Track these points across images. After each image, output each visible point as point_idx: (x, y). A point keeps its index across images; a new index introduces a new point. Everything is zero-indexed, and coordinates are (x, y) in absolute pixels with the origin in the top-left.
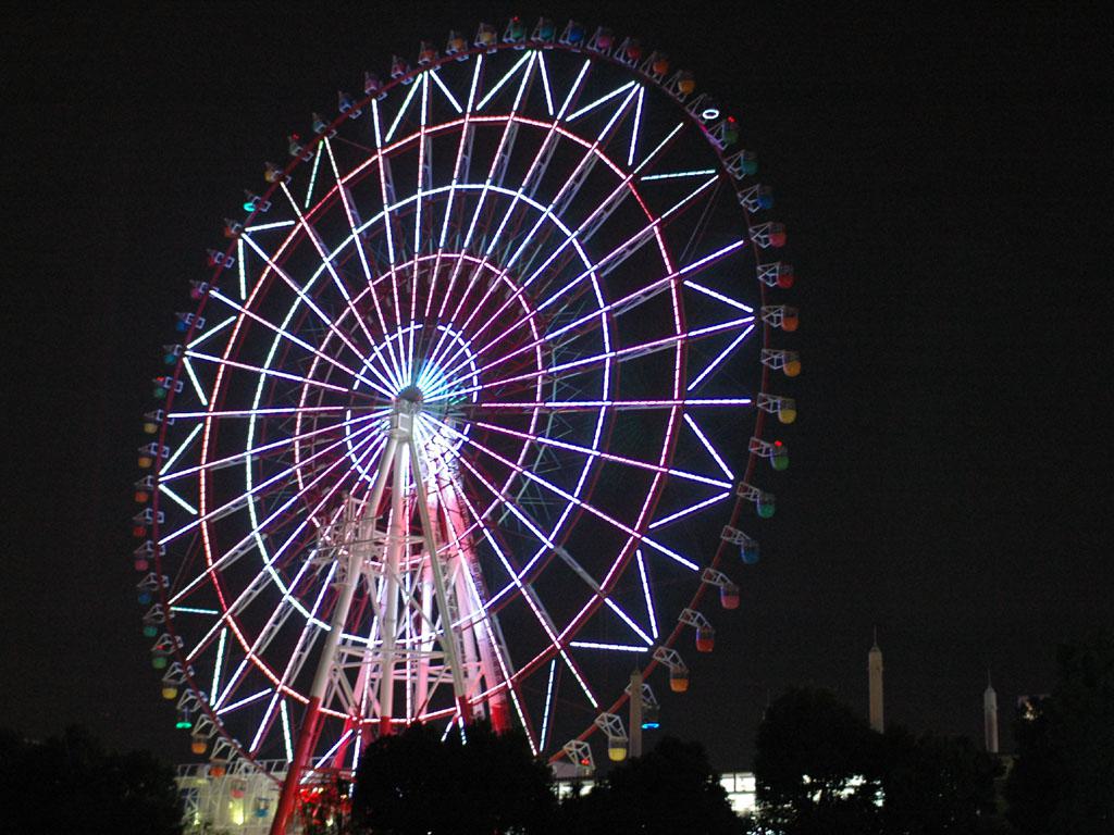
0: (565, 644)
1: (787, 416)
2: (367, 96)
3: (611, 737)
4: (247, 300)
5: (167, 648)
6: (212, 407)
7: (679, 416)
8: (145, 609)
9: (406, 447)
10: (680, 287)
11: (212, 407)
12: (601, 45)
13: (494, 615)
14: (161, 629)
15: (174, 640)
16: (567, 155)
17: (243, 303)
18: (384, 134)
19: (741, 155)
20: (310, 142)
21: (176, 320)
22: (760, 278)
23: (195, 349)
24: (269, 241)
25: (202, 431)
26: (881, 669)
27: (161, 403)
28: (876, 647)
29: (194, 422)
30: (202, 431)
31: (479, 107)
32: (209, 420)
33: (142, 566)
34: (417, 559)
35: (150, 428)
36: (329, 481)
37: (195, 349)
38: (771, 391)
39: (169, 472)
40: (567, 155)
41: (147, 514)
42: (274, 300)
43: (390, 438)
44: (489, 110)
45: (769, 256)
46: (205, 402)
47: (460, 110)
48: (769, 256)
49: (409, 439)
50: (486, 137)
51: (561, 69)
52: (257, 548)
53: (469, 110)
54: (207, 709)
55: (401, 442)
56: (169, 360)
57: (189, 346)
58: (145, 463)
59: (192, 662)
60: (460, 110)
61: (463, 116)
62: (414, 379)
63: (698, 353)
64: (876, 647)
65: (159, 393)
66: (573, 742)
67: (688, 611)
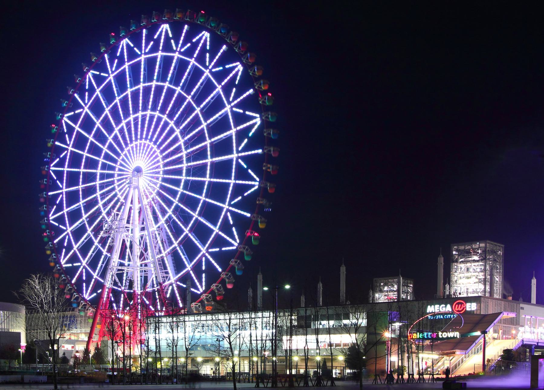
0: (207, 251)
2: (102, 53)
4: (70, 143)
6: (64, 187)
7: (237, 161)
9: (137, 190)
10: (232, 112)
11: (64, 187)
13: (181, 246)
16: (182, 65)
17: (68, 145)
18: (111, 67)
23: (54, 166)
24: (75, 119)
25: (62, 198)
26: (345, 273)
28: (343, 265)
29: (58, 195)
30: (62, 198)
32: (64, 193)
34: (143, 233)
36: (113, 207)
37: (253, 186)
39: (53, 215)
40: (182, 65)
41: (47, 233)
42: (80, 142)
43: (130, 187)
44: (151, 51)
46: (61, 186)
49: (137, 187)
50: (151, 63)
51: (176, 30)
52: (91, 238)
54: (84, 299)
55: (134, 188)
56: (44, 173)
57: (52, 165)
58: (43, 213)
59: (75, 283)
60: (139, 53)
63: (241, 135)
64: (343, 265)
67: (249, 231)
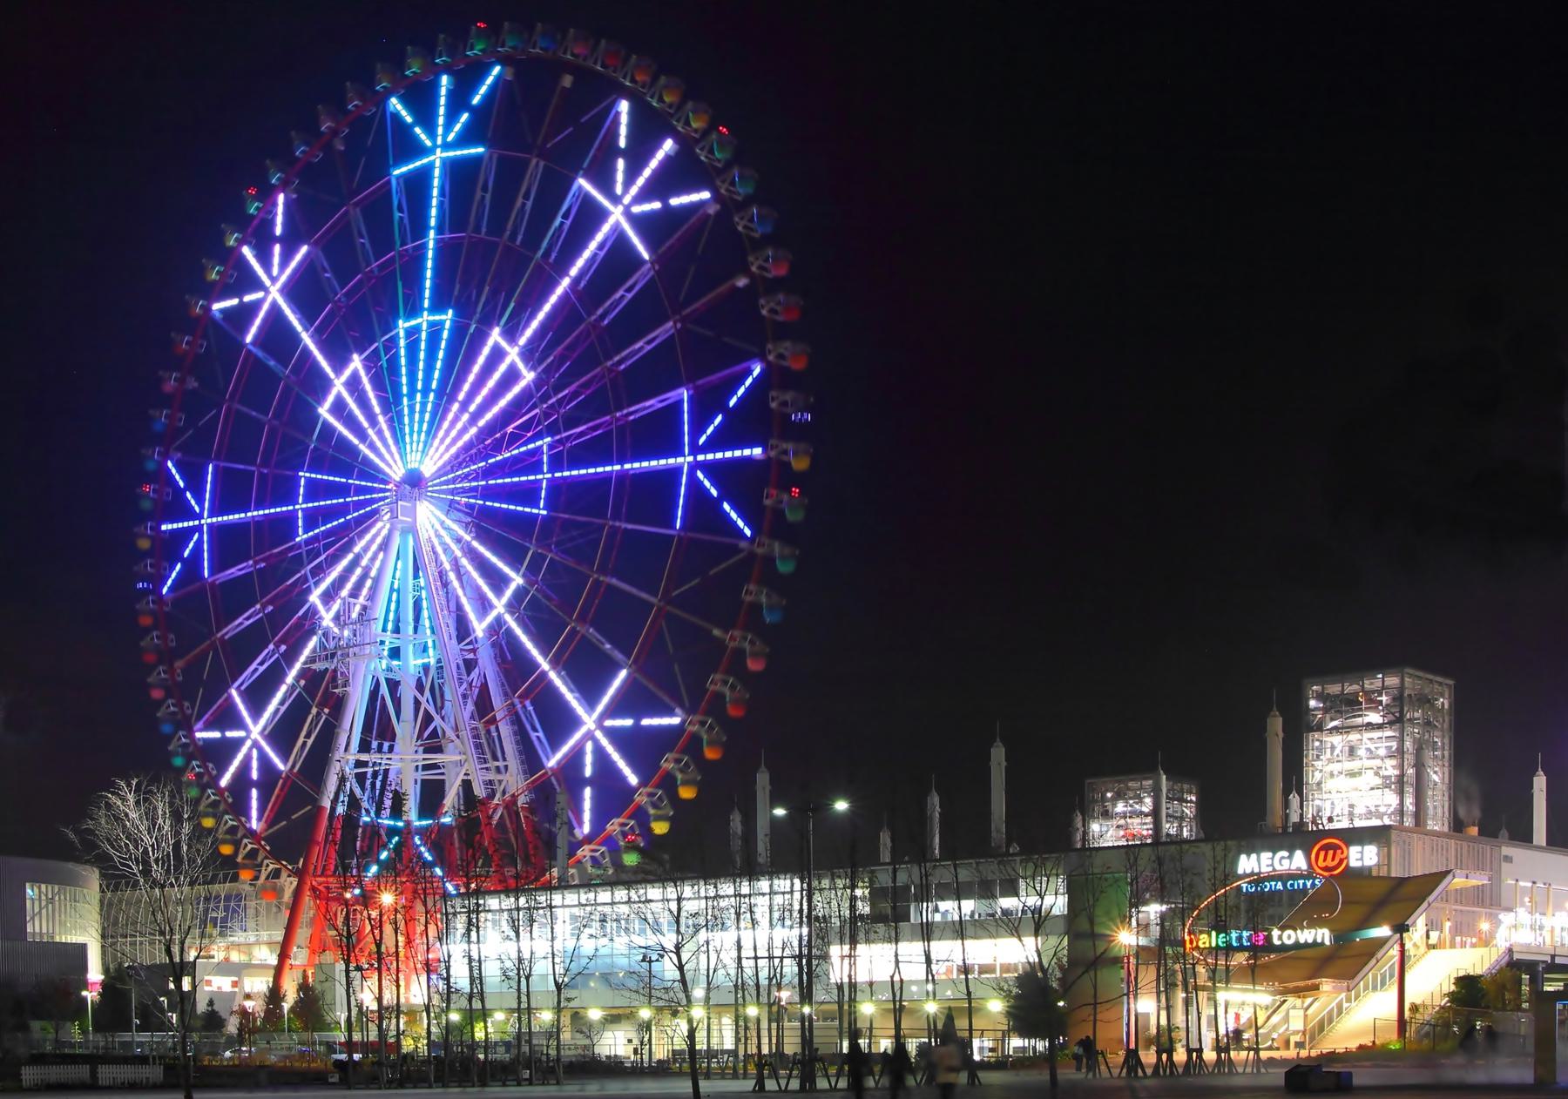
1: (800, 464)
3: (652, 811)
5: (199, 775)
8: (169, 738)
12: (576, 51)
14: (189, 758)
15: (206, 768)
19: (736, 171)
20: (267, 195)
21: (202, 271)
22: (764, 312)
25: (200, 540)
26: (1004, 764)
27: (144, 517)
28: (998, 743)
31: (451, 137)
33: (157, 694)
35: (144, 544)
38: (784, 437)
45: (773, 286)
47: (428, 143)
48: (773, 286)
53: (439, 141)
55: (404, 532)
56: (151, 466)
61: (431, 151)
62: (405, 463)
64: (998, 743)
65: (158, 427)
66: (616, 821)
67: (718, 676)
